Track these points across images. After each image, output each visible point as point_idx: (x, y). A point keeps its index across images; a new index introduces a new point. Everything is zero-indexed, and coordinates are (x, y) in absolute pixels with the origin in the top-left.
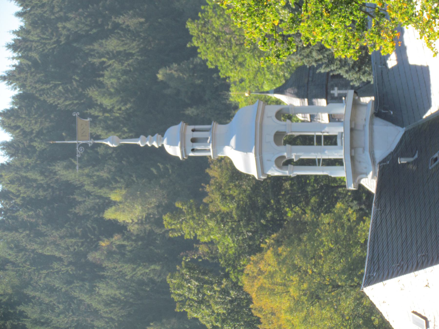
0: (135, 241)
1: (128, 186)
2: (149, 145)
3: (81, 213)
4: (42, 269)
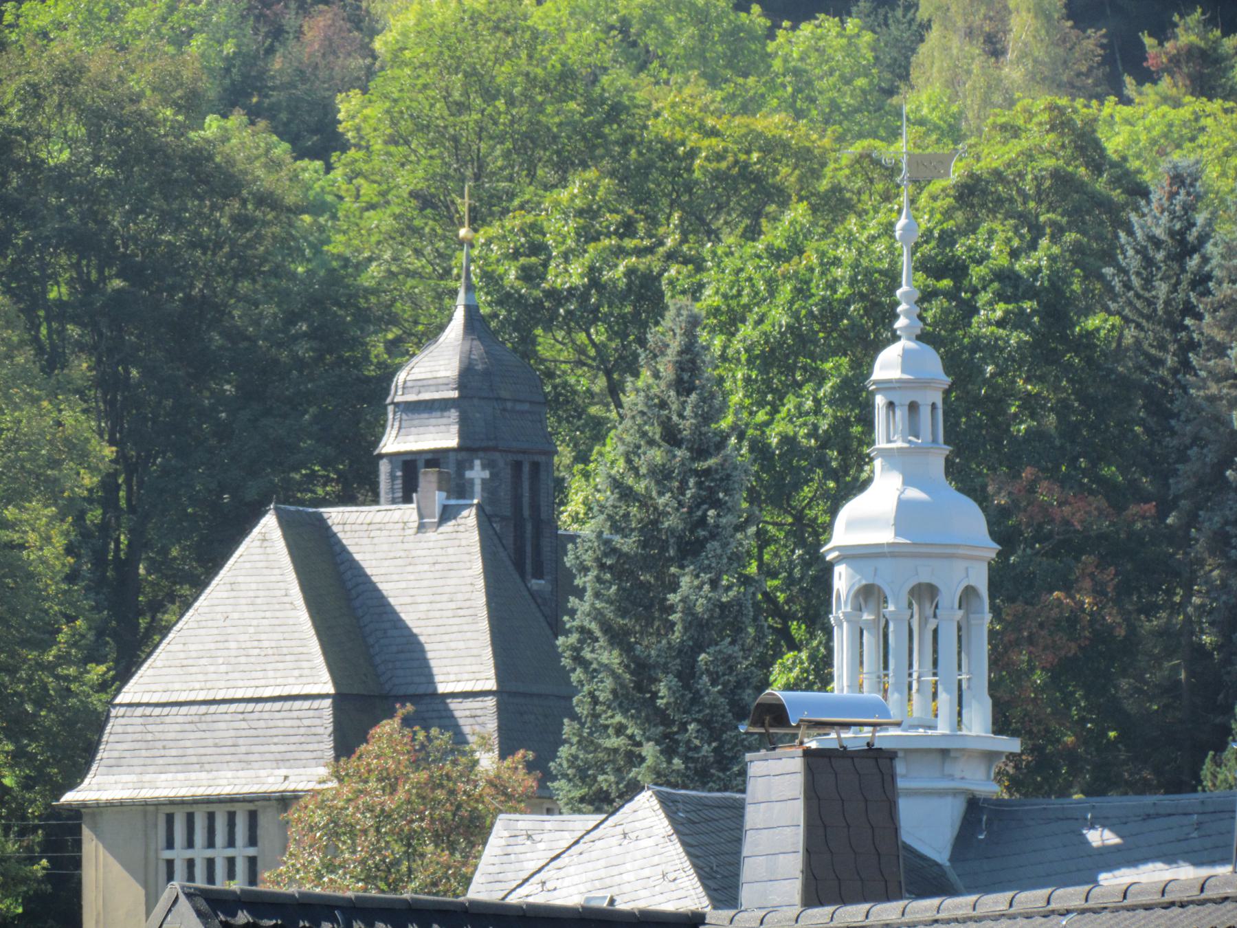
2: (899, 309)
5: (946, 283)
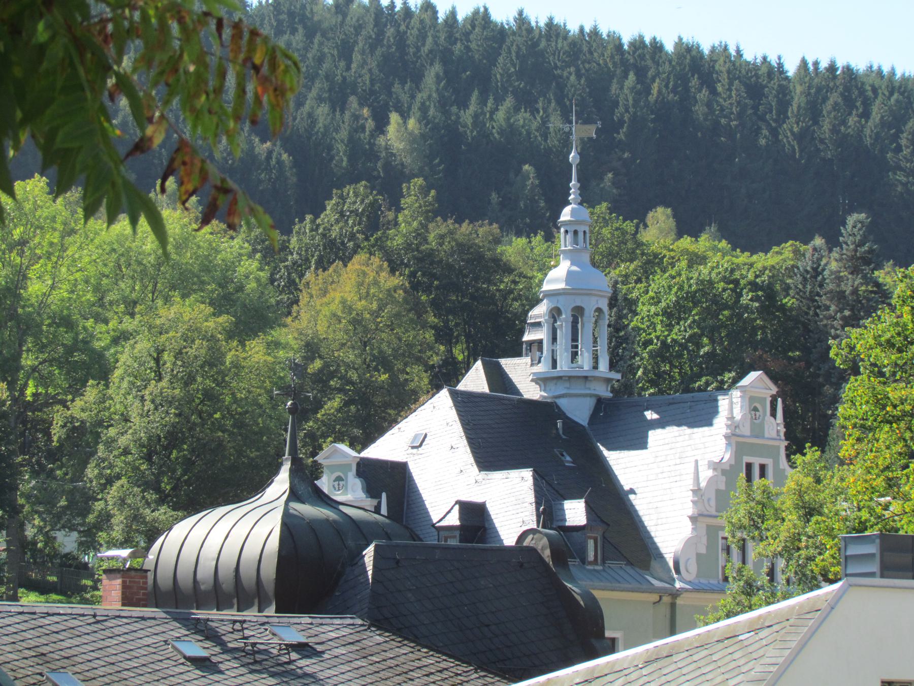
0: (369, 143)
1: (423, 136)
3: (393, 90)
4: (338, 50)
5: (731, 286)
